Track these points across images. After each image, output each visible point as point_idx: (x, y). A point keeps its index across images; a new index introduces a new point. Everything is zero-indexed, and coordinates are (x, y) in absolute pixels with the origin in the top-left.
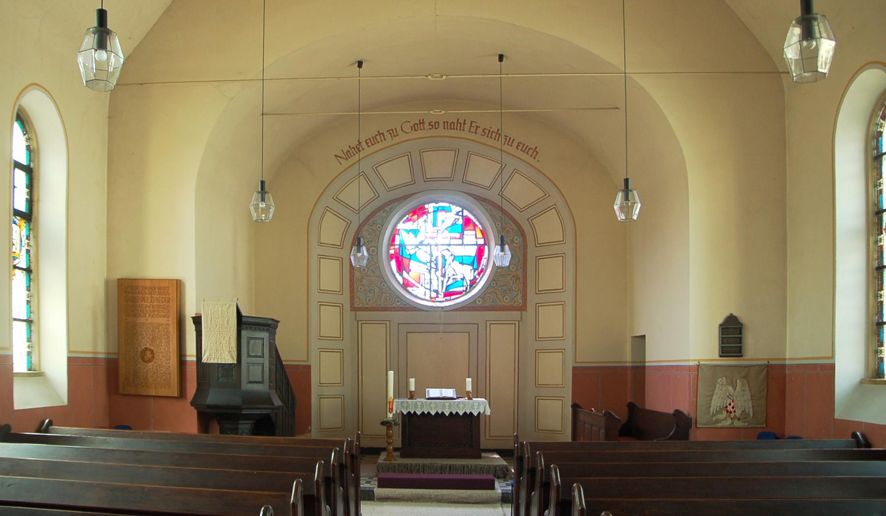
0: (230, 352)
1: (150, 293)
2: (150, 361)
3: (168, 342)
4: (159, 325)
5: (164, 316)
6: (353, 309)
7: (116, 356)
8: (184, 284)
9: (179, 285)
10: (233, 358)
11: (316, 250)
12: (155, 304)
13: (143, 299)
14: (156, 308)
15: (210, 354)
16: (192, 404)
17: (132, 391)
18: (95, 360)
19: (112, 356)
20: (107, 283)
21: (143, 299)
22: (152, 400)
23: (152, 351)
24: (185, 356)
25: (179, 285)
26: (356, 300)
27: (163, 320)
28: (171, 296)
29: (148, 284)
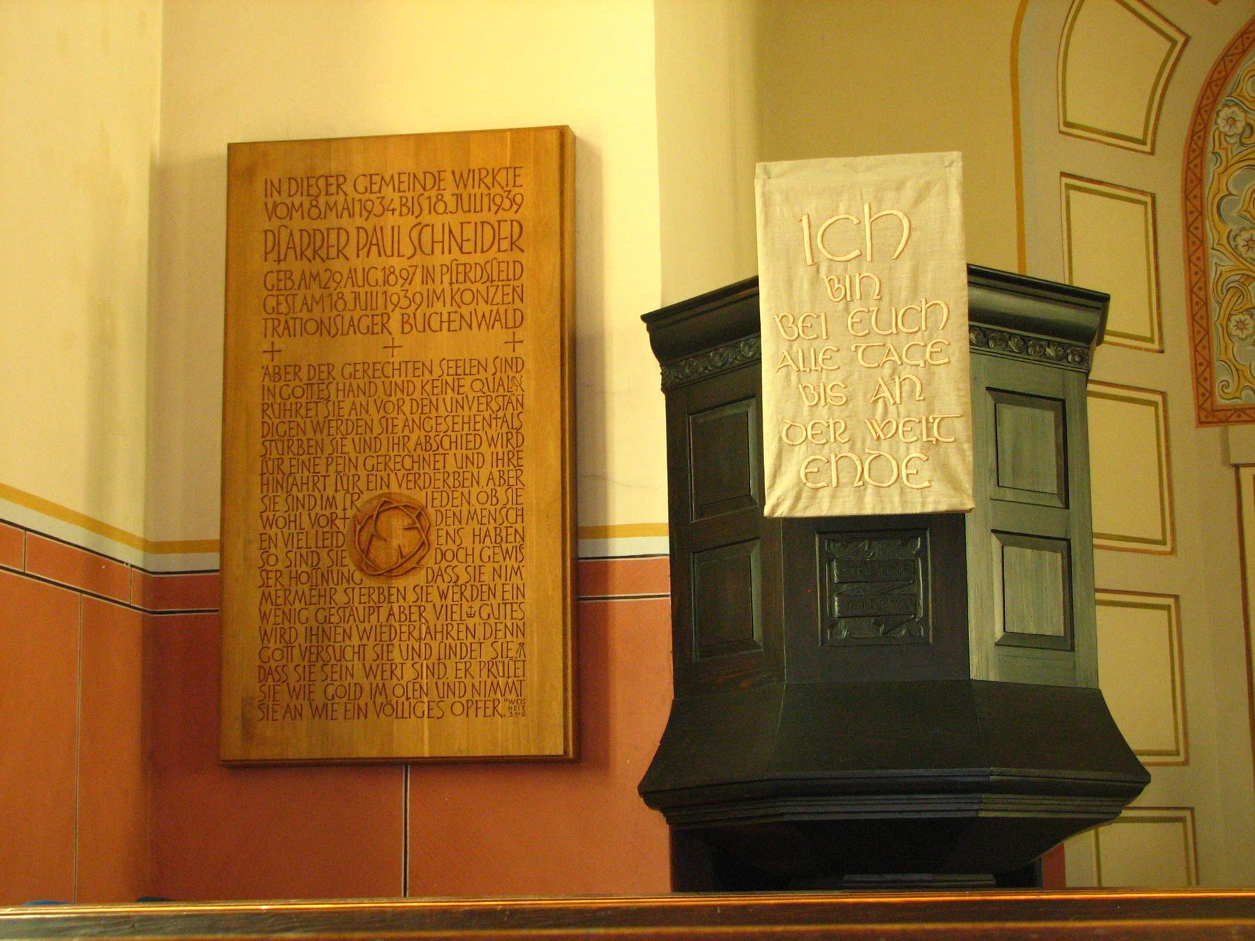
0: (931, 446)
1: (409, 207)
2: (405, 565)
3: (513, 457)
4: (460, 369)
5: (488, 322)
6: (1210, 414)
7: (211, 561)
8: (595, 158)
9: (557, 157)
10: (952, 481)
11: (1051, 155)
12: (440, 259)
13: (372, 242)
14: (443, 284)
15: (814, 470)
16: (652, 792)
17: (301, 741)
18: (96, 564)
19: (175, 562)
20: (162, 180)
21: (372, 242)
22: (405, 790)
23: (417, 515)
24: (603, 532)
25: (557, 157)
26: (1221, 376)
27: (485, 344)
28: (527, 214)
29: (401, 162)
